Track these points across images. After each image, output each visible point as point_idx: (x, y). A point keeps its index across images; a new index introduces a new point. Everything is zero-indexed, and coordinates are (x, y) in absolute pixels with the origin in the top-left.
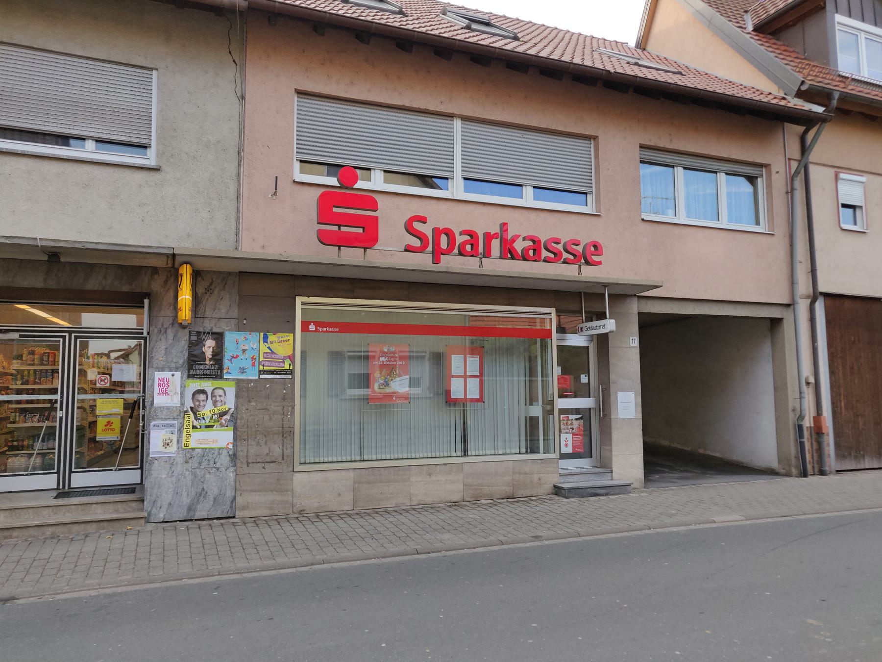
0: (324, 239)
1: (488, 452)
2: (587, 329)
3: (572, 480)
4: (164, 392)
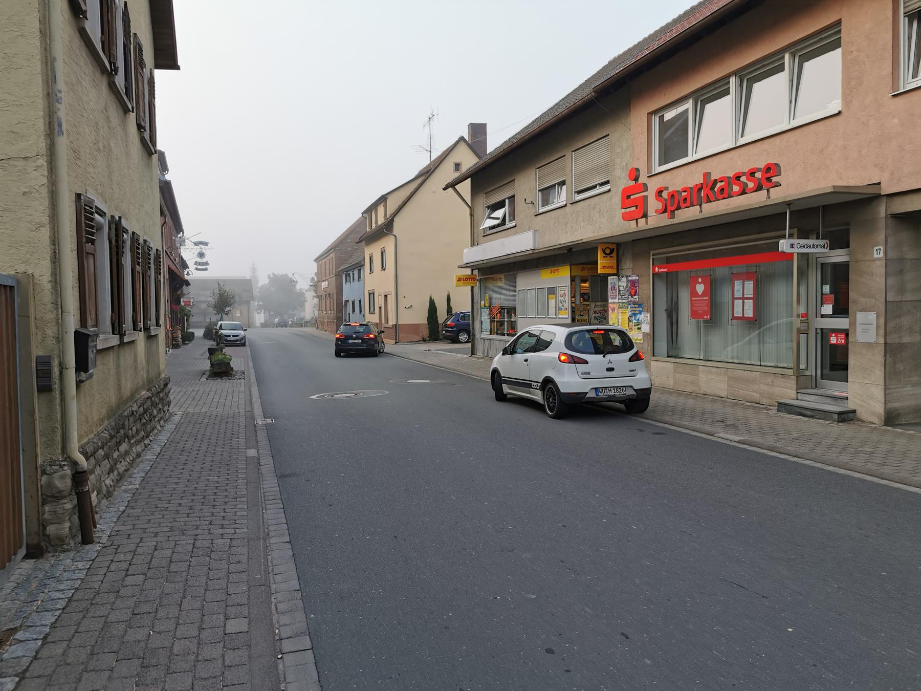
0: (626, 217)
1: (753, 363)
2: (801, 247)
3: (809, 400)
4: (865, 331)
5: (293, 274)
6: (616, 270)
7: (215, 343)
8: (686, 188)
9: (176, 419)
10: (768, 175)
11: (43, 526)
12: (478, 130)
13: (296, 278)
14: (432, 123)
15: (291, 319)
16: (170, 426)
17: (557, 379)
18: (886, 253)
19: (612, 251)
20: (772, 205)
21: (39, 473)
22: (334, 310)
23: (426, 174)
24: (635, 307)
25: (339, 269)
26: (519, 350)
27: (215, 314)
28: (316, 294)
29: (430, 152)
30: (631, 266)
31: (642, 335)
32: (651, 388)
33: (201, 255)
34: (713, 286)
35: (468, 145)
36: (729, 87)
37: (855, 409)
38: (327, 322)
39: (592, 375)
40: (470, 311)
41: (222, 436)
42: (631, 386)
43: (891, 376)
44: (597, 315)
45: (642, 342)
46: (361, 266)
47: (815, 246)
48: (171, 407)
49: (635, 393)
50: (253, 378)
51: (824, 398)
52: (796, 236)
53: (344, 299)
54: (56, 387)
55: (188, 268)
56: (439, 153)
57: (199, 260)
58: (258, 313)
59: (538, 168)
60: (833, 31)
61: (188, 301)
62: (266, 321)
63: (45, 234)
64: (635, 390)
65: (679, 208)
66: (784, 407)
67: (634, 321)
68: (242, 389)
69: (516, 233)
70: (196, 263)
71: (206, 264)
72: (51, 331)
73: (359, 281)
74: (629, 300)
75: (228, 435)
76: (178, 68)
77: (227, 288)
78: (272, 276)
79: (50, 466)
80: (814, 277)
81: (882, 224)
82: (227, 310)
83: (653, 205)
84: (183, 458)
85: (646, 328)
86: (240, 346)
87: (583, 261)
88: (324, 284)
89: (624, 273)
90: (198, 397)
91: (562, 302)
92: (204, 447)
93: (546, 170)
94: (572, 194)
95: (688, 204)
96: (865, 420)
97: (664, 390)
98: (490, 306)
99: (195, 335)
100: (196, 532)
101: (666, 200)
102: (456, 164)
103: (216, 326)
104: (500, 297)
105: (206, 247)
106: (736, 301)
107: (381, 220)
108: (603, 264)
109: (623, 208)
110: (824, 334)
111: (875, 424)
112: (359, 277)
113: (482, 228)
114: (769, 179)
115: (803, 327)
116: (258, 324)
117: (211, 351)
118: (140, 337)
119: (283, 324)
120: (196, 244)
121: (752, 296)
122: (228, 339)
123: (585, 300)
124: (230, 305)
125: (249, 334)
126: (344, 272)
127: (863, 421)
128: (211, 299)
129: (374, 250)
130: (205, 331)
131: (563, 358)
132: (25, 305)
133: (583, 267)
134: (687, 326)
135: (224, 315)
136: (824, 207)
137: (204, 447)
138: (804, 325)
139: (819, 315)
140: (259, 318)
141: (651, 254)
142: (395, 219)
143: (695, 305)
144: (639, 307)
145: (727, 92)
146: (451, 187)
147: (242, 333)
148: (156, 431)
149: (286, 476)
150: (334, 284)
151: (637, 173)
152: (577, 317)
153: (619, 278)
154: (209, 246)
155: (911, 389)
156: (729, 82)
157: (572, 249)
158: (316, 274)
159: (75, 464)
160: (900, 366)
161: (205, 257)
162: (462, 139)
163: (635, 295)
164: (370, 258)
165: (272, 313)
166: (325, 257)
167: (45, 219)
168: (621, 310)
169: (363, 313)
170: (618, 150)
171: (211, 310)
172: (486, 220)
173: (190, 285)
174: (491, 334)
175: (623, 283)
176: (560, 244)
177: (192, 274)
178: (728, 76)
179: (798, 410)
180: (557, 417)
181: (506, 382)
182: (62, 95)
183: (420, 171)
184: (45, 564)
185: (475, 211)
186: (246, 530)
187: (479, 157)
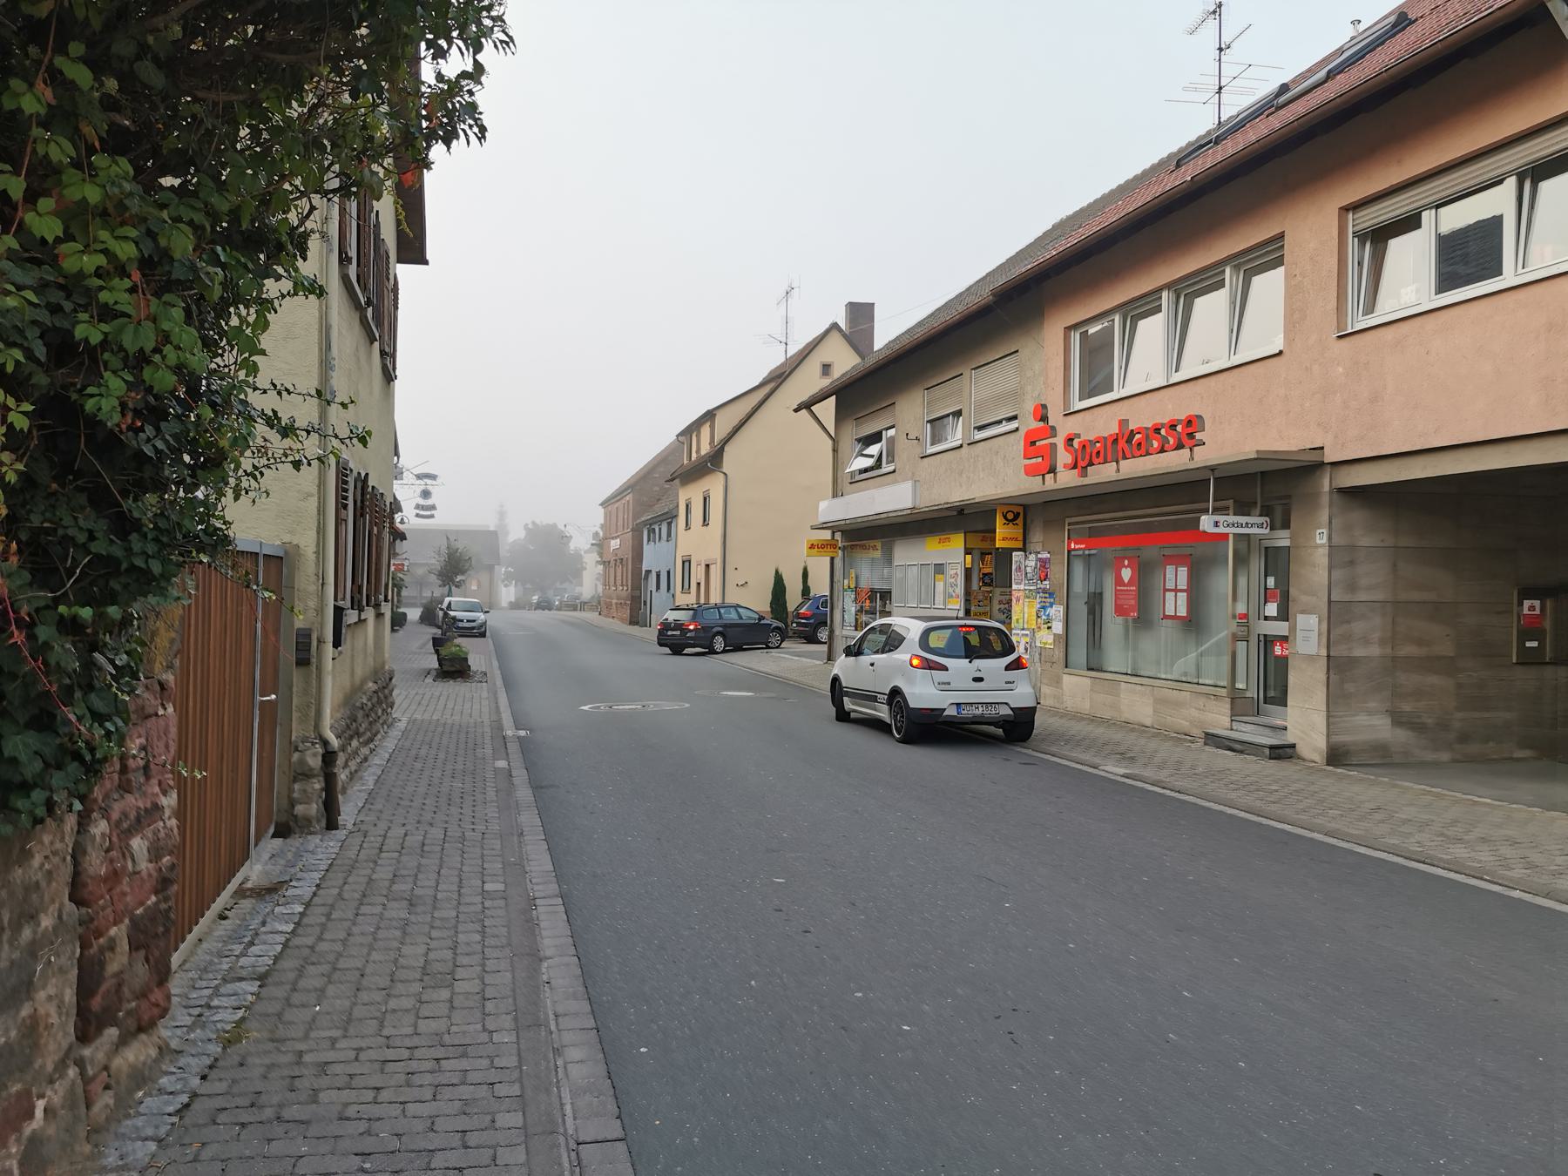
0: (1030, 471)
3: (1244, 730)
5: (565, 526)
6: (1022, 543)
7: (439, 632)
8: (1099, 437)
9: (402, 725)
10: (1190, 430)
11: (292, 804)
12: (861, 314)
13: (570, 531)
14: (789, 300)
15: (559, 598)
16: (395, 733)
17: (906, 690)
18: (1330, 538)
19: (1016, 516)
20: (1192, 469)
21: (293, 750)
22: (627, 586)
23: (778, 378)
24: (1045, 598)
25: (638, 521)
26: (866, 651)
27: (440, 586)
28: (601, 557)
29: (786, 344)
30: (1041, 539)
31: (1052, 637)
32: (1036, 707)
33: (426, 494)
34: (1145, 571)
35: (845, 336)
36: (1161, 305)
37: (1294, 742)
38: (616, 604)
39: (953, 686)
40: (828, 593)
41: (462, 746)
42: (1006, 704)
43: (1336, 699)
44: (1002, 606)
45: (1052, 647)
46: (672, 518)
47: (1250, 526)
48: (394, 709)
49: (1011, 713)
50: (499, 682)
51: (1261, 728)
52: (1231, 511)
53: (644, 568)
54: (314, 660)
55: (402, 512)
56: (801, 346)
57: (422, 502)
58: (506, 586)
59: (927, 389)
60: (1276, 246)
61: (399, 564)
62: (517, 599)
63: (313, 504)
64: (1011, 708)
65: (1091, 464)
66: (1212, 739)
67: (1044, 617)
68: (485, 694)
69: (895, 482)
70: (418, 507)
71: (433, 507)
72: (312, 603)
73: (668, 541)
74: (1038, 586)
75: (471, 745)
76: (426, 263)
77: (460, 545)
78: (530, 526)
79: (303, 742)
80: (1257, 564)
81: (1325, 499)
82: (458, 580)
83: (1064, 458)
84: (418, 765)
85: (1058, 627)
86: (476, 636)
87: (981, 527)
88: (615, 544)
89: (1032, 548)
90: (424, 702)
91: (954, 585)
92: (442, 756)
93: (937, 391)
94: (970, 431)
95: (1101, 459)
96: (1306, 757)
97: (1054, 712)
98: (856, 588)
99: (408, 617)
100: (446, 826)
101: (1076, 451)
102: (824, 365)
103: (442, 603)
104: (868, 574)
105: (434, 482)
106: (1167, 593)
107: (705, 449)
108: (1003, 534)
109: (1025, 457)
110: (1268, 641)
111: (1315, 762)
112: (669, 535)
113: (848, 470)
114: (1191, 436)
115: (1241, 632)
116: (504, 604)
117: (437, 643)
118: (369, 614)
119: (545, 605)
120: (419, 477)
121: (1185, 588)
122: (460, 625)
123: (985, 584)
124: (463, 573)
125: (493, 620)
126: (646, 525)
127: (1304, 760)
128: (433, 561)
129: (691, 494)
130: (422, 613)
131: (915, 662)
132: (292, 577)
133: (983, 537)
134: (1113, 625)
135: (453, 588)
136: (1262, 472)
137: (442, 756)
138: (1242, 629)
139: (1262, 617)
140: (507, 594)
141: (1066, 523)
142: (726, 448)
143: (1120, 597)
144: (1050, 598)
145: (1158, 310)
146: (804, 408)
147: (481, 617)
148: (379, 736)
149: (542, 787)
150: (630, 543)
151: (1044, 411)
152: (973, 608)
153: (1026, 555)
154: (439, 481)
155: (1365, 718)
156: (1161, 298)
157: (963, 510)
158: (602, 526)
159: (325, 743)
160: (1350, 687)
161: (430, 497)
162: (835, 326)
163: (1045, 580)
164: (687, 506)
165: (528, 586)
166: (618, 501)
167: (314, 490)
168: (1027, 600)
169: (672, 591)
170: (1029, 374)
171: (433, 578)
172: (856, 457)
173: (406, 539)
174: (856, 630)
175: (1032, 562)
176: (948, 503)
177: (408, 518)
178: (1160, 290)
179: (1227, 743)
180: (906, 740)
181: (847, 694)
182: (336, 362)
183: (771, 372)
184: (295, 842)
185: (840, 444)
186: (498, 828)
187: (862, 357)
